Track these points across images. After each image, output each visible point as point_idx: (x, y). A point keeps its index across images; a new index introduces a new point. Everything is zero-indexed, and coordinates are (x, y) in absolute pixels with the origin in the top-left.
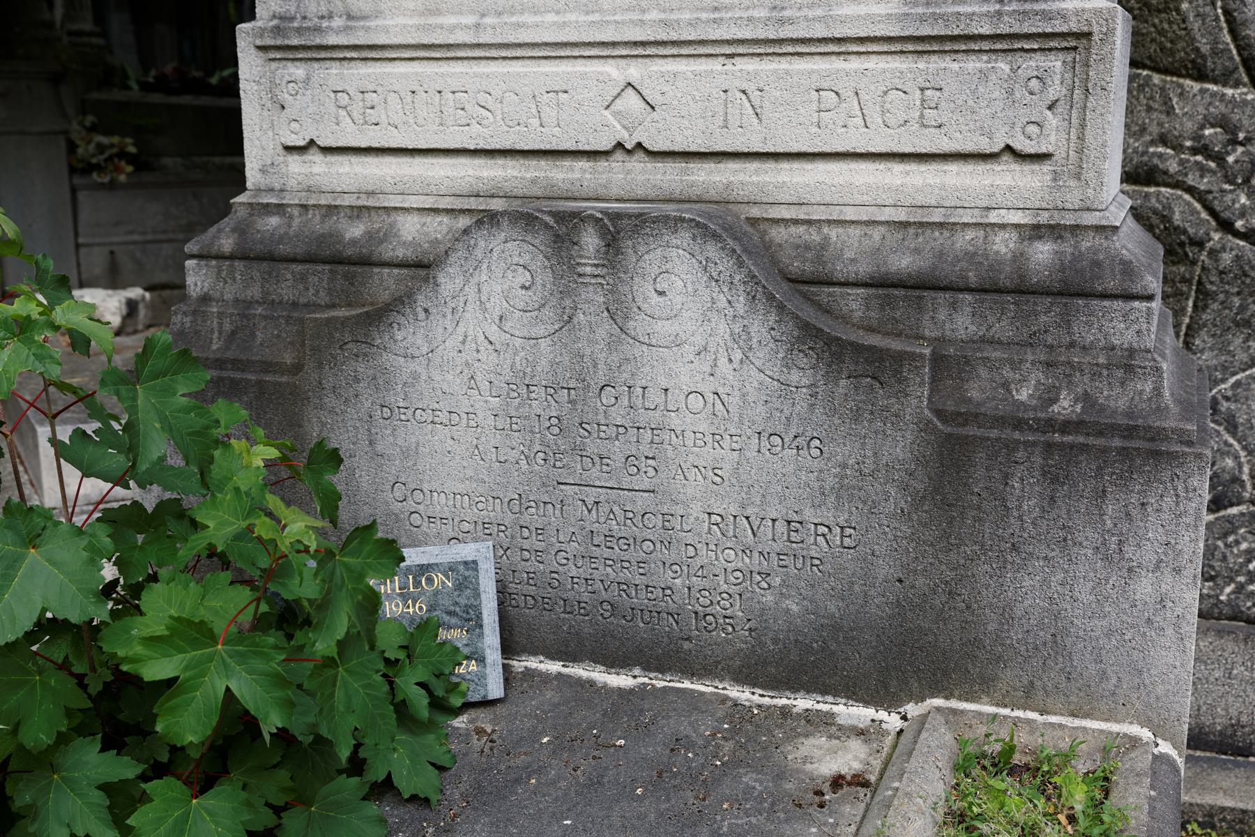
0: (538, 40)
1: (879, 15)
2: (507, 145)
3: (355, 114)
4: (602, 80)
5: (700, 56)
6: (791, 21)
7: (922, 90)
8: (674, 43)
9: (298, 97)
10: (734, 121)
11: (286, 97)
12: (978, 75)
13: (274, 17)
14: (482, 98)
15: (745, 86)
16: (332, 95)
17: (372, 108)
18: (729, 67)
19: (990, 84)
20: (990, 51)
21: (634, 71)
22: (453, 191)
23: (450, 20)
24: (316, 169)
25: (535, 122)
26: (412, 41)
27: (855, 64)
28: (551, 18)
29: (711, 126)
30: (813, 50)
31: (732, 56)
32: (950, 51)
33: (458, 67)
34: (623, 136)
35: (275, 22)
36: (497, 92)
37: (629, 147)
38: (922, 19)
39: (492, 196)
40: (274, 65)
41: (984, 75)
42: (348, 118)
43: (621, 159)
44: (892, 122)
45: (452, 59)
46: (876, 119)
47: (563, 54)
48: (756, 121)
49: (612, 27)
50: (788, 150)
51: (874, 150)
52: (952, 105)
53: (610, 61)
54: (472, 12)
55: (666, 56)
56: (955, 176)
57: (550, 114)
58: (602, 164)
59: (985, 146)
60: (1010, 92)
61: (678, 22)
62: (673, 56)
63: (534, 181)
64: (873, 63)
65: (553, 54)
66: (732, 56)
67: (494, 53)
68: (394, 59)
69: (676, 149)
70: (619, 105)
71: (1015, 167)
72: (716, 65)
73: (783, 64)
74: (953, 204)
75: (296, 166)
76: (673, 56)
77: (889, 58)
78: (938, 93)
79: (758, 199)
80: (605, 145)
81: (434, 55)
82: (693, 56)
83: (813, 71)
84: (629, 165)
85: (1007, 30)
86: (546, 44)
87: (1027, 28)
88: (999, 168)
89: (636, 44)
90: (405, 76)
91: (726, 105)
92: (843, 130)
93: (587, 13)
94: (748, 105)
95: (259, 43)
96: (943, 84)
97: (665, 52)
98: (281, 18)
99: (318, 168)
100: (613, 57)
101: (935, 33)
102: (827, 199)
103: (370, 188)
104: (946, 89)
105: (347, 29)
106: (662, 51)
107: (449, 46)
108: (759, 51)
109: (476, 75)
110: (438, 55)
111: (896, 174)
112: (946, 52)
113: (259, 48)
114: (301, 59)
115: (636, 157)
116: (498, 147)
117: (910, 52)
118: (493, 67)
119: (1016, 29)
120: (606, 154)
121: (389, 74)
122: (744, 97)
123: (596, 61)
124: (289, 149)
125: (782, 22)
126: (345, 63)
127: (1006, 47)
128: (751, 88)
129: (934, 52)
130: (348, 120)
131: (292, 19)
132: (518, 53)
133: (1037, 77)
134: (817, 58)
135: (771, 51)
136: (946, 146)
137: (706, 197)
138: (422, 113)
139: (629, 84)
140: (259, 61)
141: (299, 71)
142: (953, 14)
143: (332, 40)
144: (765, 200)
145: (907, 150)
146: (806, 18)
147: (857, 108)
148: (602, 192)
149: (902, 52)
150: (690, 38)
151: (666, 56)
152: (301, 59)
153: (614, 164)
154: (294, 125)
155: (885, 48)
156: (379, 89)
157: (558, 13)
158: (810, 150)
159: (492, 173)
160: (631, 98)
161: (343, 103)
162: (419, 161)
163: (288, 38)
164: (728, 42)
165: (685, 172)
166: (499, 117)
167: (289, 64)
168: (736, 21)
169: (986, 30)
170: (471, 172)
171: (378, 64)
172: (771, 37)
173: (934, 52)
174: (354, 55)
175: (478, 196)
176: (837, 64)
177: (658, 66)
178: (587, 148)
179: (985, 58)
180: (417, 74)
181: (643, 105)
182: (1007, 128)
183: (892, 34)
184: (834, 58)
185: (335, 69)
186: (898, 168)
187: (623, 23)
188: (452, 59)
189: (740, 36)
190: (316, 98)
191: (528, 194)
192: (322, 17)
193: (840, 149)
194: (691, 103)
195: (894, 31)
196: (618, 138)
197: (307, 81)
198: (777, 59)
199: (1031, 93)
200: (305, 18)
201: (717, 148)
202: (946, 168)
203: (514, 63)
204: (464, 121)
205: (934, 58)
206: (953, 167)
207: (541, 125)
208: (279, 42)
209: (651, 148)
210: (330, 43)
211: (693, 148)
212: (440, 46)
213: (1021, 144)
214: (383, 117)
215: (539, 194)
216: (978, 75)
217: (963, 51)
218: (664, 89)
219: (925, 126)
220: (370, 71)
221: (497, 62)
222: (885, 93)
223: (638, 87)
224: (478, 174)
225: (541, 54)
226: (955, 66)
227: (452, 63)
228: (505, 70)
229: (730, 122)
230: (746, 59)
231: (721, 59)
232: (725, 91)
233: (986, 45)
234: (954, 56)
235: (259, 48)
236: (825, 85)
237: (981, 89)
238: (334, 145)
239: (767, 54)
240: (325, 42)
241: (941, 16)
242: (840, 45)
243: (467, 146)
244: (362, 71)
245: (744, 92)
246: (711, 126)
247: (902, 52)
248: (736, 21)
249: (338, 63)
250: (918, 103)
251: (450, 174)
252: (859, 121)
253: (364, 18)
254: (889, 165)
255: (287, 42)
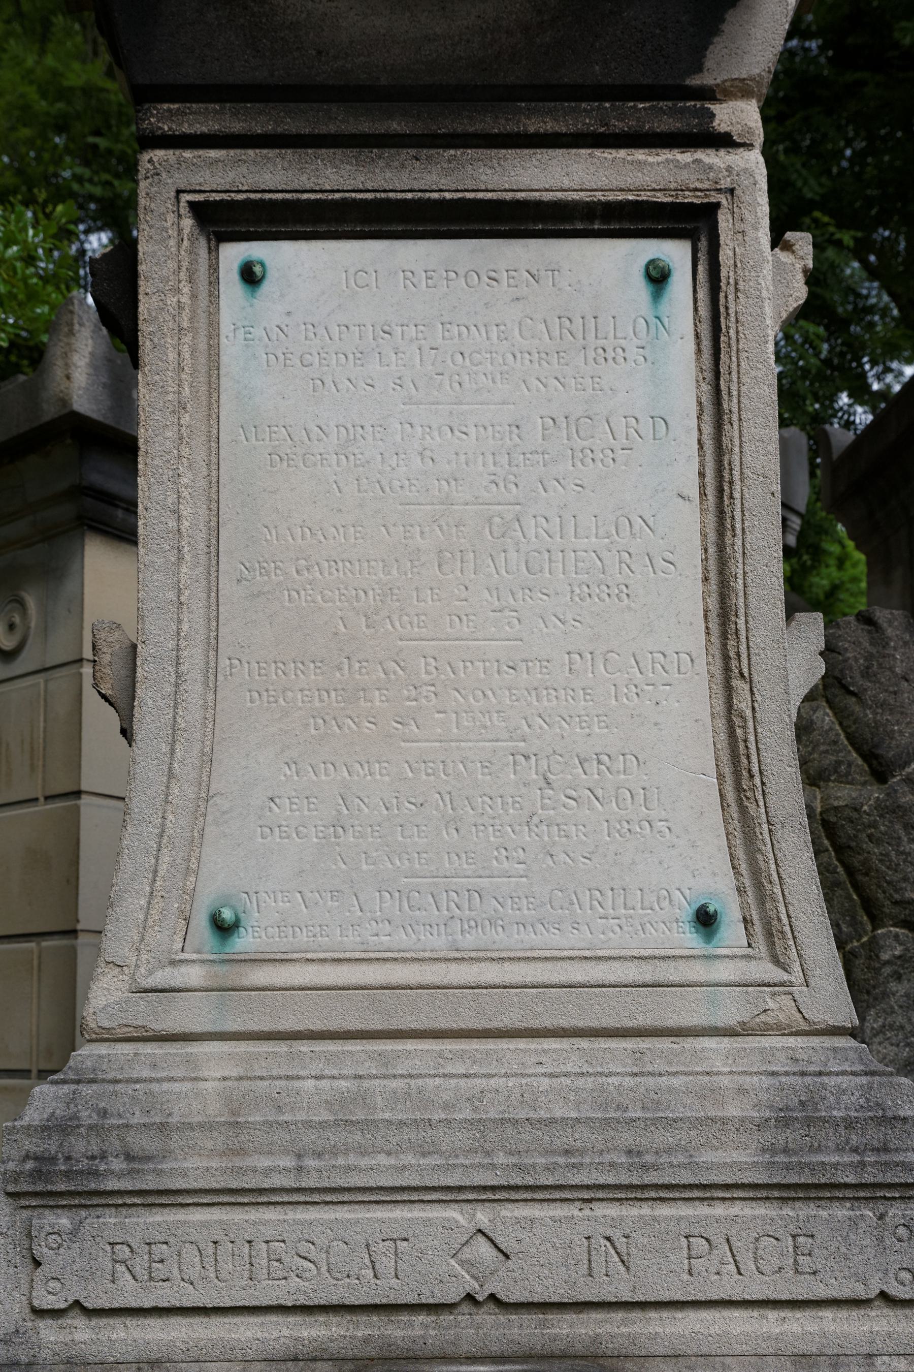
0: (372, 1184)
1: (746, 1163)
2: (335, 1300)
3: (138, 1270)
4: (449, 1226)
5: (555, 1200)
6: (655, 1167)
7: (794, 1237)
8: (527, 1188)
9: (62, 1250)
10: (599, 1269)
11: (42, 1251)
12: (848, 1223)
13: (27, 1157)
14: (303, 1248)
15: (609, 1232)
16: (108, 1248)
17: (162, 1261)
18: (587, 1212)
19: (861, 1231)
20: (854, 1198)
21: (482, 1216)
22: (265, 1355)
23: (265, 1162)
24: (79, 1336)
25: (369, 1273)
26: (215, 1185)
27: (719, 1210)
28: (382, 1160)
29: (574, 1275)
30: (677, 1195)
31: (590, 1201)
32: (815, 1198)
33: (270, 1214)
34: (472, 1285)
35: (30, 1165)
36: (322, 1241)
37: (480, 1298)
38: (788, 1167)
39: (314, 1360)
40: (25, 1214)
41: (853, 1223)
42: (127, 1275)
43: (467, 1311)
44: (766, 1268)
45: (262, 1204)
46: (749, 1266)
47: (399, 1198)
48: (622, 1269)
49: (459, 1171)
50: (659, 1299)
51: (750, 1298)
52: (825, 1252)
53: (452, 1205)
54: (285, 1152)
55: (517, 1201)
56: (830, 1323)
57: (386, 1264)
58: (446, 1318)
59: (861, 1292)
60: (881, 1239)
61: (534, 1166)
62: (526, 1200)
63: (366, 1340)
64: (736, 1209)
65: (388, 1199)
66: (590, 1201)
67: (316, 1198)
68: (188, 1205)
69: (536, 1300)
70: (467, 1253)
71: (887, 1311)
72: (572, 1210)
73: (645, 1210)
74: (835, 1352)
75: (49, 1333)
76: (526, 1200)
77: (754, 1204)
78: (810, 1240)
79: (630, 1352)
80: (453, 1295)
81: (240, 1199)
82: (548, 1200)
83: (681, 1218)
84: (478, 1319)
85: (872, 1180)
86: (381, 1189)
87: (889, 1178)
88: (873, 1314)
89: (485, 1188)
90: (203, 1224)
91: (589, 1251)
92: (716, 1277)
93: (424, 1155)
94: (613, 1252)
95: (11, 1188)
96: (814, 1231)
97: (517, 1197)
98: (36, 1158)
99: (82, 1333)
100: (456, 1201)
101: (803, 1181)
102: (705, 1350)
103: (154, 1357)
104: (818, 1236)
105: (132, 1173)
106: (513, 1195)
107: (261, 1191)
108: (619, 1196)
109: (296, 1222)
110: (246, 1200)
111: (772, 1323)
112: (810, 1198)
113: (10, 1195)
114: (63, 1207)
115: (485, 1308)
116: (323, 1302)
117: (775, 1198)
118: (312, 1214)
119: (880, 1179)
120: (449, 1307)
121: (185, 1222)
122: (608, 1244)
123: (437, 1205)
124: (39, 1313)
125: (646, 1167)
126: (124, 1211)
127: (869, 1195)
128: (616, 1235)
129: (799, 1199)
130: (128, 1276)
131: (53, 1160)
132: (346, 1197)
133: (904, 1225)
134: (680, 1203)
135: (633, 1196)
136: (823, 1292)
137: (572, 1351)
138: (226, 1266)
139: (480, 1231)
140: (7, 1210)
141: (64, 1221)
142: (818, 1163)
143: (112, 1184)
144: (637, 1353)
145: (784, 1297)
146: (671, 1165)
147: (729, 1254)
148: (449, 1350)
149: (767, 1198)
150: (546, 1183)
151: (517, 1201)
152: (63, 1207)
153: (460, 1318)
154: (52, 1284)
155: (751, 1194)
156: (172, 1240)
157: (389, 1154)
158: (683, 1299)
159: (314, 1333)
160: (484, 1249)
161: (121, 1257)
162: (215, 1321)
163: (52, 1183)
164: (588, 1187)
165: (544, 1324)
166: (324, 1269)
167: (47, 1212)
168: (598, 1166)
169: (851, 1179)
170: (286, 1332)
171: (166, 1210)
172: (635, 1182)
173: (799, 1199)
174: (137, 1200)
175: (296, 1359)
176: (703, 1210)
177: (508, 1212)
178: (431, 1301)
179: (848, 1205)
180: (221, 1221)
181: (495, 1252)
182: (881, 1275)
183: (760, 1182)
184: (697, 1203)
185: (110, 1218)
186: (772, 1315)
187: (472, 1166)
188: (262, 1204)
189: (602, 1181)
190: (86, 1252)
191: (359, 1355)
192: (93, 1158)
193: (715, 1297)
194: (551, 1250)
195: (762, 1179)
196: (468, 1289)
197: (74, 1233)
198: (638, 1204)
199: (900, 1240)
200: (68, 1158)
201: (581, 1298)
202: (820, 1314)
203: (339, 1208)
204: (280, 1274)
205: (798, 1204)
206: (828, 1314)
207: (376, 1276)
208: (39, 1188)
209: (505, 1299)
210: (109, 1188)
211: (555, 1299)
212: (251, 1191)
213: (895, 1290)
214: (176, 1271)
215: (373, 1354)
216: (848, 1223)
217: (828, 1198)
218: (521, 1236)
219: (801, 1273)
220: (158, 1218)
221: (318, 1207)
222: (757, 1239)
223: (491, 1234)
224: (296, 1334)
225: (373, 1198)
226: (824, 1214)
227: (261, 1209)
228: (333, 1217)
229: (595, 1270)
230: (604, 1204)
231: (578, 1204)
232: (588, 1238)
233: (849, 1193)
234: (818, 1203)
235: (10, 1195)
236: (696, 1232)
237: (852, 1236)
238: (107, 1306)
239: (627, 1199)
240: (102, 1187)
241: (807, 1165)
242: (706, 1191)
243: (283, 1302)
244: (150, 1220)
245: (608, 1239)
246: (574, 1275)
247: (767, 1198)
248: (598, 1166)
249: (113, 1210)
250: (791, 1249)
251: (259, 1335)
252: (732, 1267)
253: (148, 1159)
254: (762, 1312)
255: (53, 1188)
